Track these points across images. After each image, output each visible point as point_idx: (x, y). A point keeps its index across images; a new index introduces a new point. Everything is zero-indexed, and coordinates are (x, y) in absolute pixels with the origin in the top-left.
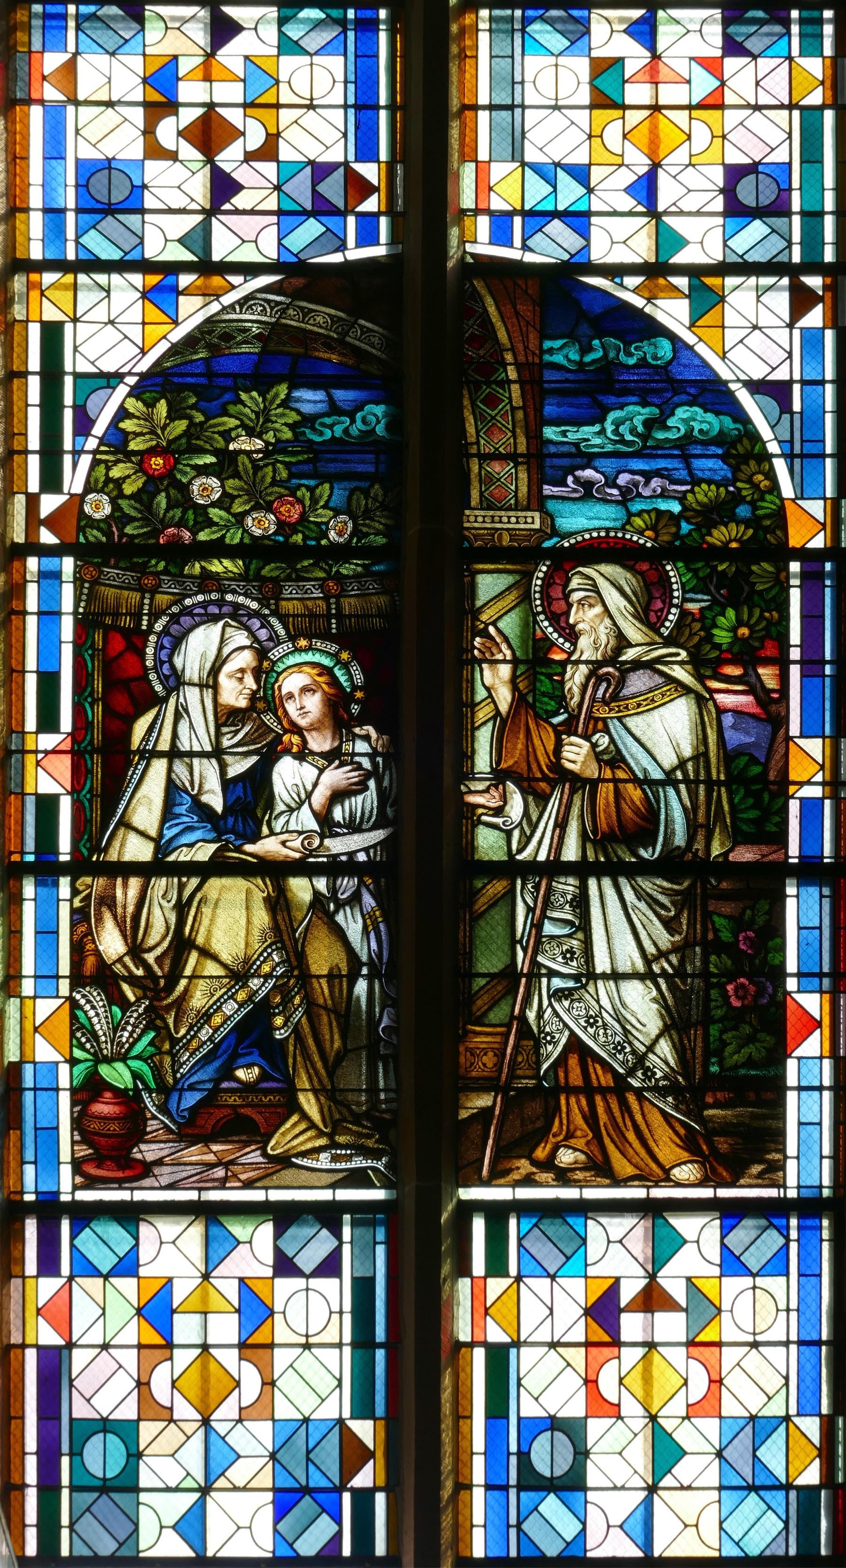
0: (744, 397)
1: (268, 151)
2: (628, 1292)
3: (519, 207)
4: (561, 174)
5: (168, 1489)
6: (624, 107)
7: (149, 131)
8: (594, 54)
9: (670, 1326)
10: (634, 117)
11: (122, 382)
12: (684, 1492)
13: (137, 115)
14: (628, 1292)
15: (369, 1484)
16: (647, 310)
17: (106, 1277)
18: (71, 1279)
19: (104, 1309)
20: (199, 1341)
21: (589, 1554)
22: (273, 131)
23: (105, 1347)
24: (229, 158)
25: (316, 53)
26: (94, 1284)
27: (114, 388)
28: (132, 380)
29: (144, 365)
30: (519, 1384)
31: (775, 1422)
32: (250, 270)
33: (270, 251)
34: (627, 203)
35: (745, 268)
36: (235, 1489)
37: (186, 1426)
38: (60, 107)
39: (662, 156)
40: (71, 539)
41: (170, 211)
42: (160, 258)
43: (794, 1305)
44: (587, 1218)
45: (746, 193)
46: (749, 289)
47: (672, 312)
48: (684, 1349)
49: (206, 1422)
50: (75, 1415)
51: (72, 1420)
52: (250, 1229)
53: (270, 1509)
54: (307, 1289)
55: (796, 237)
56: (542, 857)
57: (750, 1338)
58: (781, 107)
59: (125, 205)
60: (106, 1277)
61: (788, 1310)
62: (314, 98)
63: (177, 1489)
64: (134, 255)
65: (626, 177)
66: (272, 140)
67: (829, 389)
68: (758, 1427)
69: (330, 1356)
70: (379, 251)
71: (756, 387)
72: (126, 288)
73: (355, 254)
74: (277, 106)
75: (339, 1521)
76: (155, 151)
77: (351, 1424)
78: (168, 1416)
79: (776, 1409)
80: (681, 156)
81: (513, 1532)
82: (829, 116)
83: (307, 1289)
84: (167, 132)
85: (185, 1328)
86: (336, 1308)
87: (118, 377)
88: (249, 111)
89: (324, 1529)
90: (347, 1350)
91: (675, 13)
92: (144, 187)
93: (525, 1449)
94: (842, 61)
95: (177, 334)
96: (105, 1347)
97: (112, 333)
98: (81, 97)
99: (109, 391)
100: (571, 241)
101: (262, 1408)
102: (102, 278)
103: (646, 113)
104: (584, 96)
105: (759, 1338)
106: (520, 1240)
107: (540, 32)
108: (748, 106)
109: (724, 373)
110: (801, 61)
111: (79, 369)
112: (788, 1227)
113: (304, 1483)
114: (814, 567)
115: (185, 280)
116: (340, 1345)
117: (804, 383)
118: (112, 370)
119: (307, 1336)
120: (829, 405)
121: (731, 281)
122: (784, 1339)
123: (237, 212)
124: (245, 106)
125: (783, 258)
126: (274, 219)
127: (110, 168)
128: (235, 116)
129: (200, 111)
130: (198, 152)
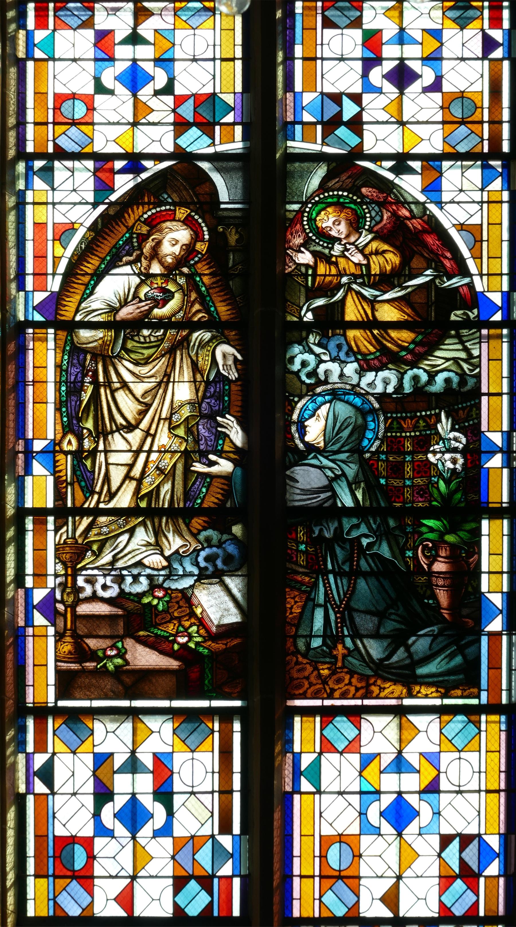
1: (168, 89)
2: (119, 761)
3: (320, 120)
5: (111, 877)
7: (365, 75)
12: (378, 879)
13: (358, 66)
14: (119, 761)
15: (230, 873)
17: (341, 753)
18: (320, 754)
19: (340, 772)
20: (131, 791)
22: (440, 74)
23: (74, 794)
24: (146, 93)
26: (334, 757)
30: (54, 817)
32: (158, 158)
35: (456, 157)
36: (151, 877)
37: (121, 840)
40: (51, 318)
42: (105, 151)
43: (483, 769)
44: (94, 719)
45: (458, 111)
46: (457, 167)
49: (134, 838)
50: (56, 834)
51: (55, 837)
52: (116, 725)
53: (171, 889)
55: (486, 136)
56: (92, 506)
57: (190, 789)
58: (478, 59)
59: (83, 121)
60: (341, 753)
62: (207, 55)
63: (116, 877)
64: (87, 150)
65: (382, 101)
66: (439, 79)
68: (194, 842)
69: (207, 799)
71: (461, 227)
75: (477, 895)
76: (100, 88)
78: (110, 833)
79: (206, 831)
81: (317, 902)
82: (506, 64)
83: (193, 759)
84: (376, 76)
89: (204, 899)
90: (216, 795)
91: (373, 3)
93: (323, 854)
94: (513, 32)
96: (74, 794)
98: (57, 57)
100: (353, 140)
101: (166, 830)
102: (69, 164)
105: (462, 789)
106: (54, 731)
107: (333, 16)
108: (458, 59)
112: (480, 722)
113: (191, 873)
115: (119, 165)
116: (212, 792)
119: (459, 786)
121: (446, 164)
122: (211, 790)
124: (423, 59)
125: (478, 150)
126: (441, 126)
127: (463, 97)
129: (397, 62)
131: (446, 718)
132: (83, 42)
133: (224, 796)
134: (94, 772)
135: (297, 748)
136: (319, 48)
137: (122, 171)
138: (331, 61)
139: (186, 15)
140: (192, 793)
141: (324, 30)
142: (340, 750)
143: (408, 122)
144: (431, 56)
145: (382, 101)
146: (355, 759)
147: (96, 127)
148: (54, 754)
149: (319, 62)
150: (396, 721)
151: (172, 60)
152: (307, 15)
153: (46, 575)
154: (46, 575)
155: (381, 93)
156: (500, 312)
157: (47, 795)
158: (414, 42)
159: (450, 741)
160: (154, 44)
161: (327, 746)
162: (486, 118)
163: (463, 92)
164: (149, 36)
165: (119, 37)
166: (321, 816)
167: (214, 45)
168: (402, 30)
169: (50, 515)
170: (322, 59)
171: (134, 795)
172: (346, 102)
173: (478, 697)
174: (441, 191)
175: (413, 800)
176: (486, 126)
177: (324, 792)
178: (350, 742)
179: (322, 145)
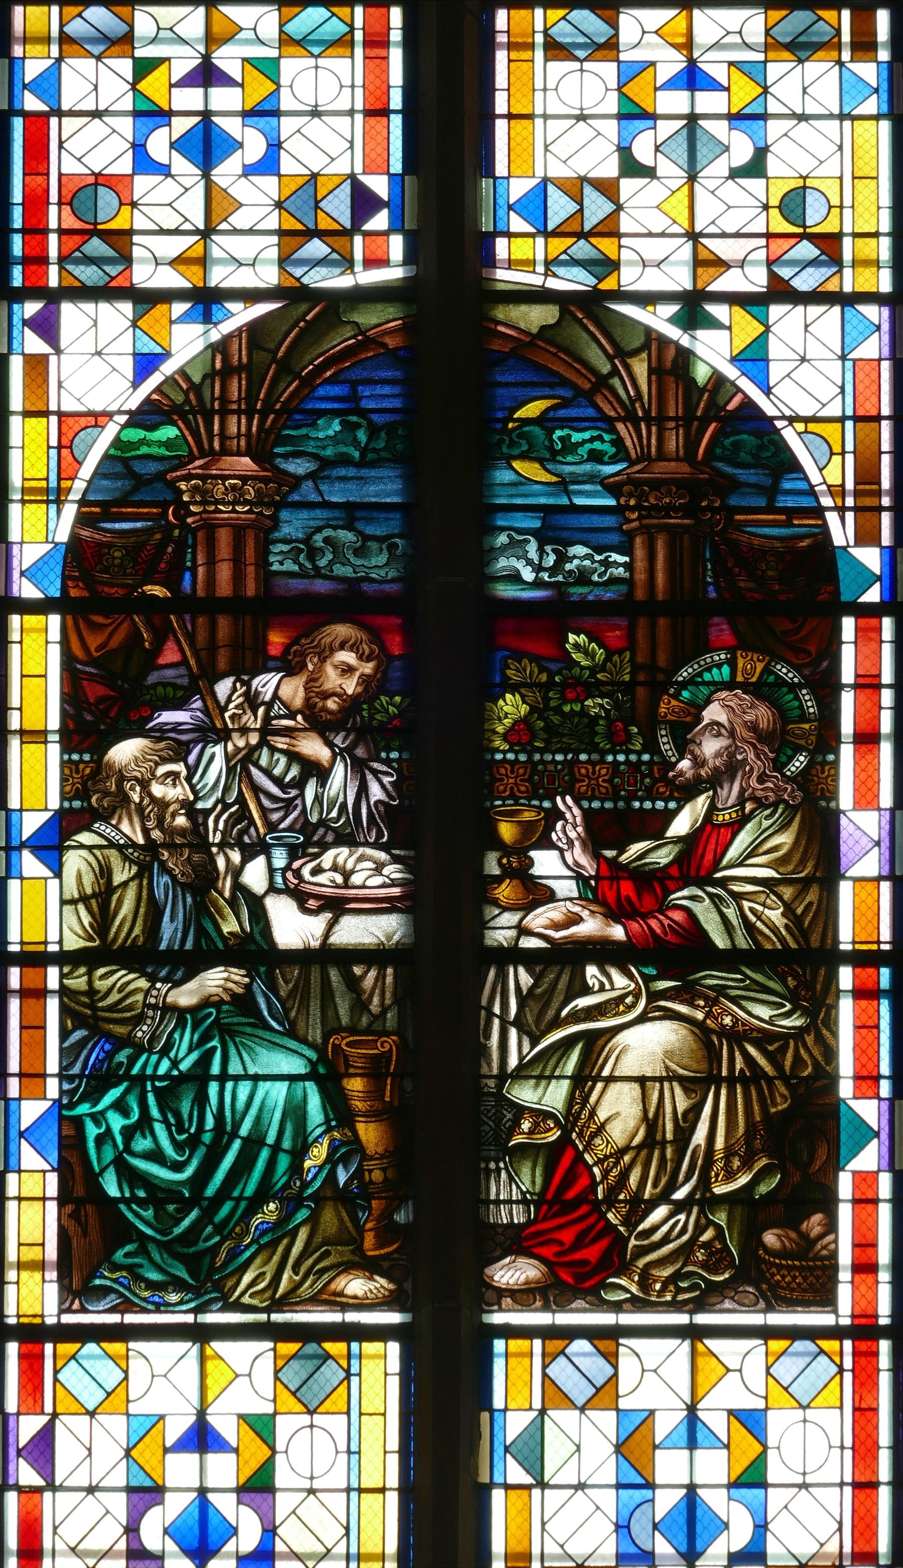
0: (789, 435)
1: (268, 164)
4: (588, 190)
6: (653, 117)
8: (138, 53)
9: (223, 1470)
10: (666, 128)
17: (582, 1409)
18: (543, 1412)
20: (686, 1481)
22: (761, 144)
24: (226, 172)
25: (585, 59)
27: (103, 427)
33: (269, 276)
38: (43, 117)
48: (613, 1491)
54: (312, 1478)
57: (799, 1480)
58: (831, 116)
60: (582, 1409)
61: (842, 1447)
67: (886, 428)
76: (144, 162)
77: (39, 1482)
80: (720, 167)
83: (805, 1421)
85: (670, 1466)
88: (249, 121)
97: (96, 363)
98: (65, 107)
103: (199, 119)
104: (612, 105)
108: (794, 116)
109: (769, 410)
110: (853, 66)
117: (857, 419)
118: (99, 408)
120: (886, 445)
123: (236, 232)
126: (763, 242)
128: (232, 126)
130: (230, 165)
131: (777, 1345)
133: (862, 1495)
136: (539, 95)
137: (184, 318)
138: (555, 118)
139: (817, 34)
140: (312, 1491)
141: (549, 64)
143: (701, 235)
144: (747, 111)
145: (654, 191)
147: (624, 241)
148: (55, 1415)
149: (539, 122)
151: (621, 117)
153: (44, 1076)
154: (44, 1076)
156: (877, 585)
157: (528, 1487)
158: (714, 85)
159: (786, 1389)
161: (555, 1396)
164: (233, 69)
167: (353, 86)
168: (692, 63)
170: (545, 117)
172: (591, 196)
174: (766, 360)
177: (62, 1488)
178: (598, 1390)
179: (546, 275)
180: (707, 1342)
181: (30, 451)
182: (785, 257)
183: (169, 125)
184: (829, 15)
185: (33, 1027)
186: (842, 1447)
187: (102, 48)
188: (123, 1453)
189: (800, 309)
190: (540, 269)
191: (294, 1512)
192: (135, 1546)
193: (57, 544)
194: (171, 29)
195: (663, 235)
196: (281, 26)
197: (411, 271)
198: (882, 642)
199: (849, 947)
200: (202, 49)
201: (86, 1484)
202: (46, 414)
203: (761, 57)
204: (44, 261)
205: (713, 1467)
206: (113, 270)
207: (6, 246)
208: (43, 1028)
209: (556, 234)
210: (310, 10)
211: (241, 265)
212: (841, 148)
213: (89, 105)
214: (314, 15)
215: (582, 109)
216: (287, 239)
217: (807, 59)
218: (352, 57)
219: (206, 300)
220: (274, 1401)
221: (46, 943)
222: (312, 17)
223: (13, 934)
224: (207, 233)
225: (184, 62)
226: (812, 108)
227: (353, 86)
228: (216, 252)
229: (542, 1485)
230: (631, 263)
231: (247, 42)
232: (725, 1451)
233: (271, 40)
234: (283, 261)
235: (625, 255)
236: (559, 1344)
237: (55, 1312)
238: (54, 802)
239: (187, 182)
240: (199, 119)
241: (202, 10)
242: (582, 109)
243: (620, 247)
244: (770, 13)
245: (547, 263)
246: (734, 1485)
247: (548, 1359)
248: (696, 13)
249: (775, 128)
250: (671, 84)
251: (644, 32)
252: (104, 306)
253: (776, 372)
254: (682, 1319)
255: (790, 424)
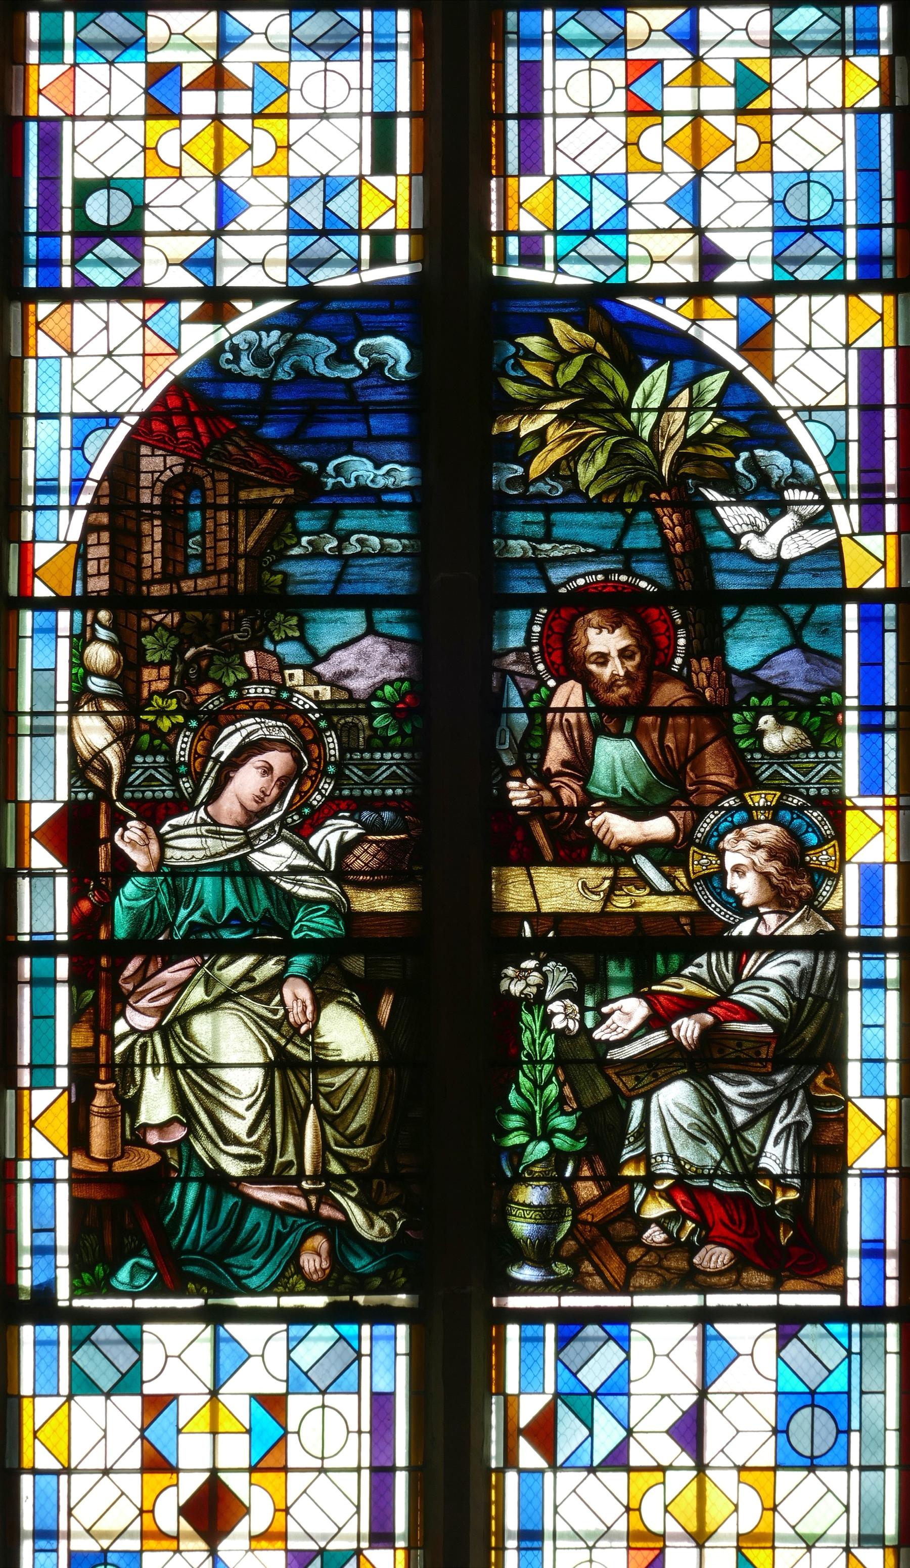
6: (661, 114)
8: (631, 55)
10: (672, 124)
11: (121, 420)
16: (692, 332)
18: (70, 1398)
21: (774, 1325)
23: (106, 1472)
26: (93, 1403)
27: (114, 428)
28: (133, 420)
29: (144, 404)
31: (351, 179)
32: (258, 295)
33: (278, 275)
34: (667, 218)
39: (703, 165)
41: (174, 233)
47: (720, 334)
55: (851, 252)
57: (317, 1464)
58: (834, 111)
61: (360, 1432)
65: (665, 188)
70: (405, 270)
72: (124, 317)
73: (372, 275)
74: (287, 116)
77: (542, 1463)
80: (726, 162)
83: (323, 1406)
86: (354, 1427)
87: (119, 417)
92: (146, 207)
94: (898, 60)
95: (180, 366)
98: (78, 113)
99: (110, 431)
103: (689, 119)
104: (619, 102)
108: (798, 110)
109: (773, 398)
111: (76, 410)
114: (873, 609)
118: (110, 410)
121: (781, 302)
125: (836, 276)
126: (283, 239)
130: (235, 167)
131: (298, 1330)
132: (127, 84)
134: (143, 1430)
135: (512, 1387)
137: (195, 318)
142: (106, 1390)
143: (706, 229)
146: (132, 1405)
147: (632, 238)
150: (696, 1331)
152: (389, 36)
155: (662, 172)
157: (542, 1471)
158: (239, 86)
160: (252, 89)
162: (851, 220)
163: (808, 172)
164: (244, 73)
165: (189, 74)
166: (556, 1512)
169: (893, 950)
170: (360, 115)
171: (214, 1471)
173: (842, 1290)
175: (237, 1483)
176: (851, 234)
178: (123, 1375)
180: (718, 1326)
181: (45, 449)
182: (302, 257)
183: (662, 124)
184: (352, 16)
185: (44, 1017)
186: (360, 1432)
187: (595, 50)
188: (138, 1433)
189: (804, 300)
190: (550, 265)
191: (574, 1491)
192: (636, 1526)
193: (69, 543)
194: (183, 34)
195: (670, 230)
196: (772, 27)
197: (418, 268)
198: (884, 631)
199: (26, 938)
200: (213, 54)
201: (103, 1467)
202: (55, 416)
203: (285, 57)
204: (57, 263)
205: (235, 1452)
206: (609, 269)
207: (21, 248)
208: (53, 1017)
209: (564, 232)
210: (801, 11)
211: (251, 264)
212: (360, 146)
213: (101, 110)
214: (806, 15)
215: (591, 107)
216: (779, 235)
217: (810, 55)
218: (361, 60)
219: (217, 303)
220: (287, 1381)
221: (54, 933)
222: (804, 17)
223: (24, 926)
224: (218, 233)
225: (195, 66)
226: (816, 103)
227: (554, 89)
228: (225, 252)
229: (554, 1467)
230: (639, 260)
231: (257, 46)
232: (247, 1436)
233: (764, 41)
234: (777, 260)
235: (634, 251)
236: (85, 1329)
237: (67, 1296)
238: (63, 794)
239: (198, 183)
240: (689, 119)
241: (213, 15)
242: (325, 108)
243: (628, 243)
244: (295, 14)
245: (557, 260)
246: (253, 1469)
247: (75, 1345)
248: (703, 13)
249: (780, 122)
250: (197, 85)
251: (171, 34)
252: (115, 306)
253: (781, 361)
254: (691, 1300)
255: (795, 414)
